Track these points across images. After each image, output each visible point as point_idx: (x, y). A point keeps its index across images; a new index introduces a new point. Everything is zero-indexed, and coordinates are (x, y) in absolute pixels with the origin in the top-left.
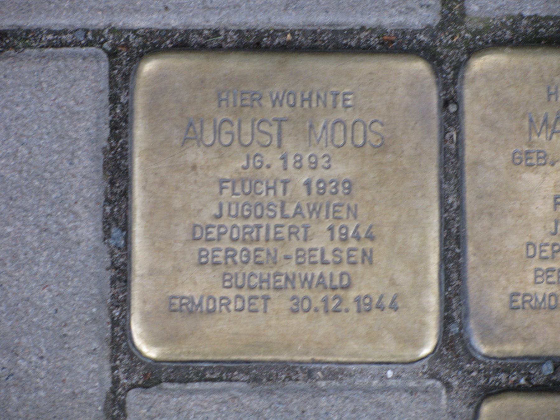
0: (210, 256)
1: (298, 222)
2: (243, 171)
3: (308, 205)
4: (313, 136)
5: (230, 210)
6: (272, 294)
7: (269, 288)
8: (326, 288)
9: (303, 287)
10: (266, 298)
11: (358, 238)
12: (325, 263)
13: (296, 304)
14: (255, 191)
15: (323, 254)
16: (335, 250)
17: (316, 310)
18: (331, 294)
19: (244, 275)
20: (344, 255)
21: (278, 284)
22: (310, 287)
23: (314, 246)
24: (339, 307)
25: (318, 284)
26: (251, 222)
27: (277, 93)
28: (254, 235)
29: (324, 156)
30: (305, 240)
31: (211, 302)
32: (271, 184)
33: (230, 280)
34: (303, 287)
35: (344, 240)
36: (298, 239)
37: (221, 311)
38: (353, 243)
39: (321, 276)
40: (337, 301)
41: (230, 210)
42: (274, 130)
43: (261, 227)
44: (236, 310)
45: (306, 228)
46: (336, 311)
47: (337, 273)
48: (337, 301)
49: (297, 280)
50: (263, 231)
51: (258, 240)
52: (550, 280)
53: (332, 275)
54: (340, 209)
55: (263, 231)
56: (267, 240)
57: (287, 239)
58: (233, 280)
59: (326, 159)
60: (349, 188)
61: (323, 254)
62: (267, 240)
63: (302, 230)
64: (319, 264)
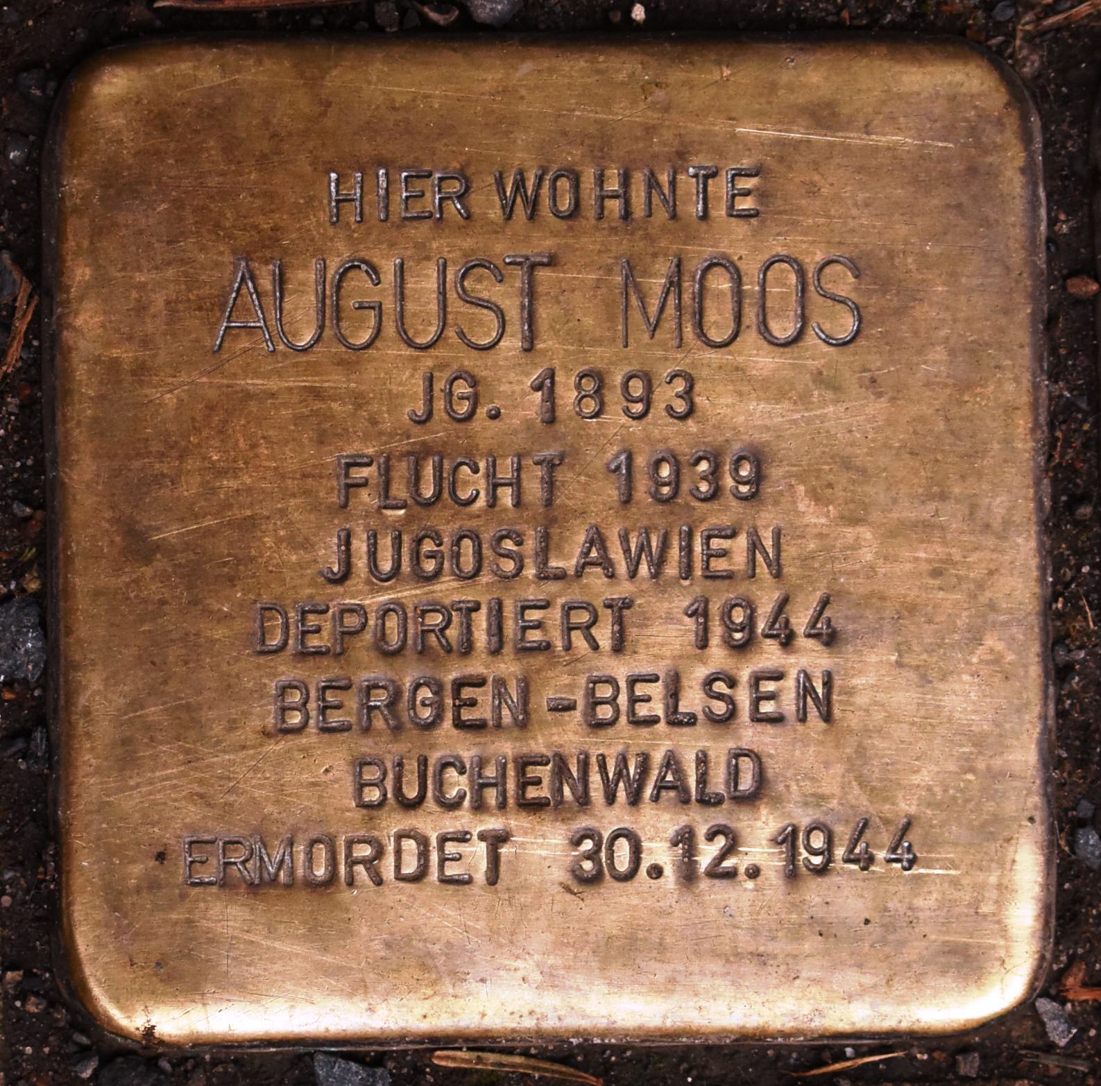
0: (623, 700)
1: (597, 585)
2: (416, 429)
3: (625, 539)
4: (636, 315)
5: (373, 555)
6: (516, 822)
7: (502, 806)
8: (686, 801)
9: (611, 799)
10: (496, 841)
11: (787, 641)
12: (678, 720)
13: (592, 856)
14: (453, 493)
15: (674, 693)
16: (709, 682)
17: (656, 872)
18: (702, 823)
19: (423, 762)
20: (743, 698)
21: (532, 793)
22: (635, 799)
23: (645, 669)
24: (728, 863)
25: (661, 787)
26: (447, 589)
27: (521, 173)
28: (453, 633)
29: (674, 377)
30: (619, 647)
31: (321, 852)
32: (506, 471)
33: (379, 784)
34: (611, 799)
35: (742, 649)
36: (595, 647)
37: (351, 883)
38: (770, 655)
39: (672, 762)
40: (721, 841)
41: (373, 555)
42: (508, 297)
43: (477, 607)
44: (400, 877)
45: (620, 609)
46: (719, 874)
47: (719, 751)
48: (721, 841)
49: (595, 779)
50: (481, 620)
51: (467, 648)
52: (335, 718)
53: (703, 760)
54: (725, 544)
55: (481, 620)
56: (496, 652)
57: (559, 644)
58: (389, 784)
59: (680, 385)
60: (758, 479)
61: (674, 693)
62: (496, 652)
63: (607, 617)
64: (662, 727)
